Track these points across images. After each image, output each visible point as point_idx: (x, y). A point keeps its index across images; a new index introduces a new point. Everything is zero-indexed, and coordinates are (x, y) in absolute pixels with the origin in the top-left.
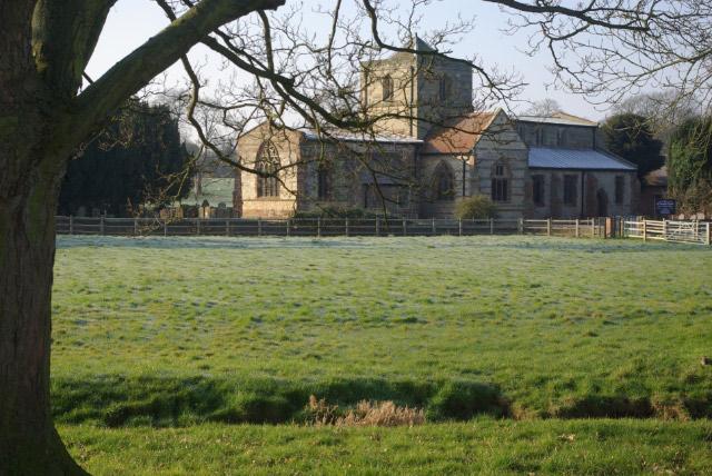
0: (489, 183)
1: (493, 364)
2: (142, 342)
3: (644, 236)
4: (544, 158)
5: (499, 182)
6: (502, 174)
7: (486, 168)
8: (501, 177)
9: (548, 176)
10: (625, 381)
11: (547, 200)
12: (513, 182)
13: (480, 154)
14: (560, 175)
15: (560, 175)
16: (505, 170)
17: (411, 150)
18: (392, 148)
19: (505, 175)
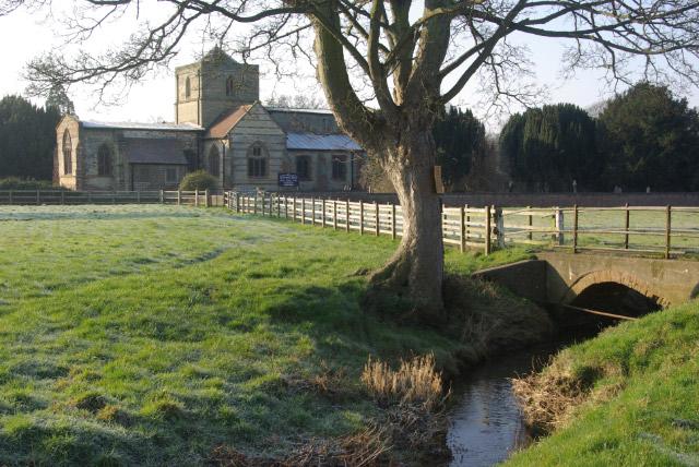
0: (245, 162)
1: (102, 364)
2: (657, 357)
3: (333, 224)
4: (297, 142)
5: (257, 162)
6: (259, 154)
7: (241, 150)
8: (257, 157)
9: (315, 157)
10: (181, 405)
11: (314, 174)
12: (271, 162)
13: (235, 138)
14: (328, 156)
15: (328, 156)
16: (262, 151)
17: (194, 137)
18: (174, 135)
19: (263, 155)
